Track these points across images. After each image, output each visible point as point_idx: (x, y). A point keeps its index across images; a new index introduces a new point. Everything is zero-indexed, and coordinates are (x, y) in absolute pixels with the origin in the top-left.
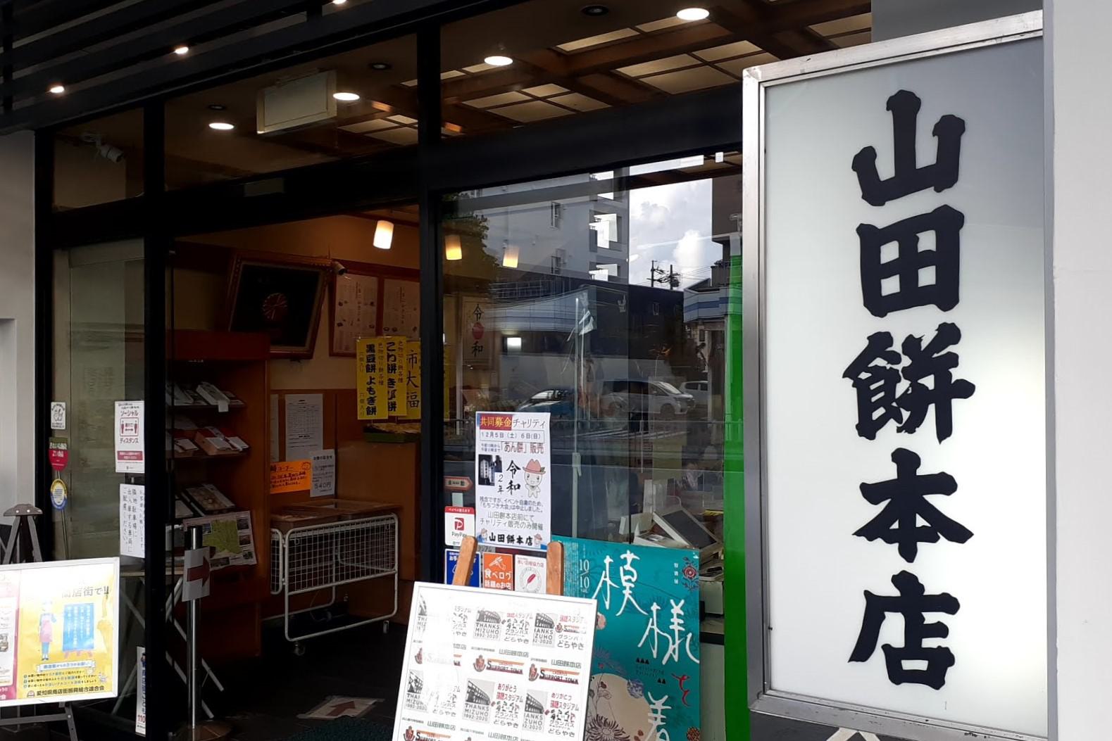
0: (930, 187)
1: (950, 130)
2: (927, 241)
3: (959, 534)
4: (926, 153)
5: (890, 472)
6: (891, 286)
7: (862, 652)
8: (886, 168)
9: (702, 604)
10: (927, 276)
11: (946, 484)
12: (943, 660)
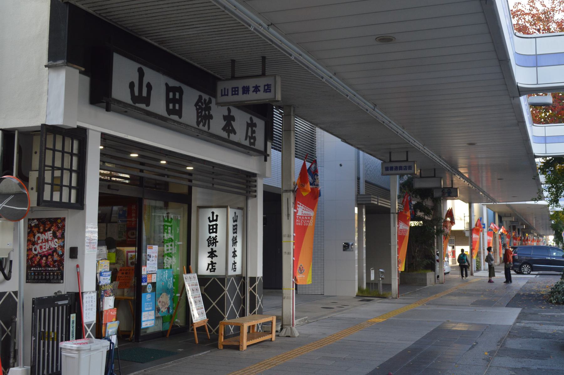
0: (171, 193)
1: (217, 216)
2: (215, 227)
3: (217, 256)
4: (215, 218)
5: (210, 250)
6: (211, 231)
7: (207, 270)
8: (211, 219)
9: (266, 160)
10: (215, 230)
11: (215, 251)
12: (215, 269)
